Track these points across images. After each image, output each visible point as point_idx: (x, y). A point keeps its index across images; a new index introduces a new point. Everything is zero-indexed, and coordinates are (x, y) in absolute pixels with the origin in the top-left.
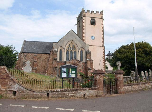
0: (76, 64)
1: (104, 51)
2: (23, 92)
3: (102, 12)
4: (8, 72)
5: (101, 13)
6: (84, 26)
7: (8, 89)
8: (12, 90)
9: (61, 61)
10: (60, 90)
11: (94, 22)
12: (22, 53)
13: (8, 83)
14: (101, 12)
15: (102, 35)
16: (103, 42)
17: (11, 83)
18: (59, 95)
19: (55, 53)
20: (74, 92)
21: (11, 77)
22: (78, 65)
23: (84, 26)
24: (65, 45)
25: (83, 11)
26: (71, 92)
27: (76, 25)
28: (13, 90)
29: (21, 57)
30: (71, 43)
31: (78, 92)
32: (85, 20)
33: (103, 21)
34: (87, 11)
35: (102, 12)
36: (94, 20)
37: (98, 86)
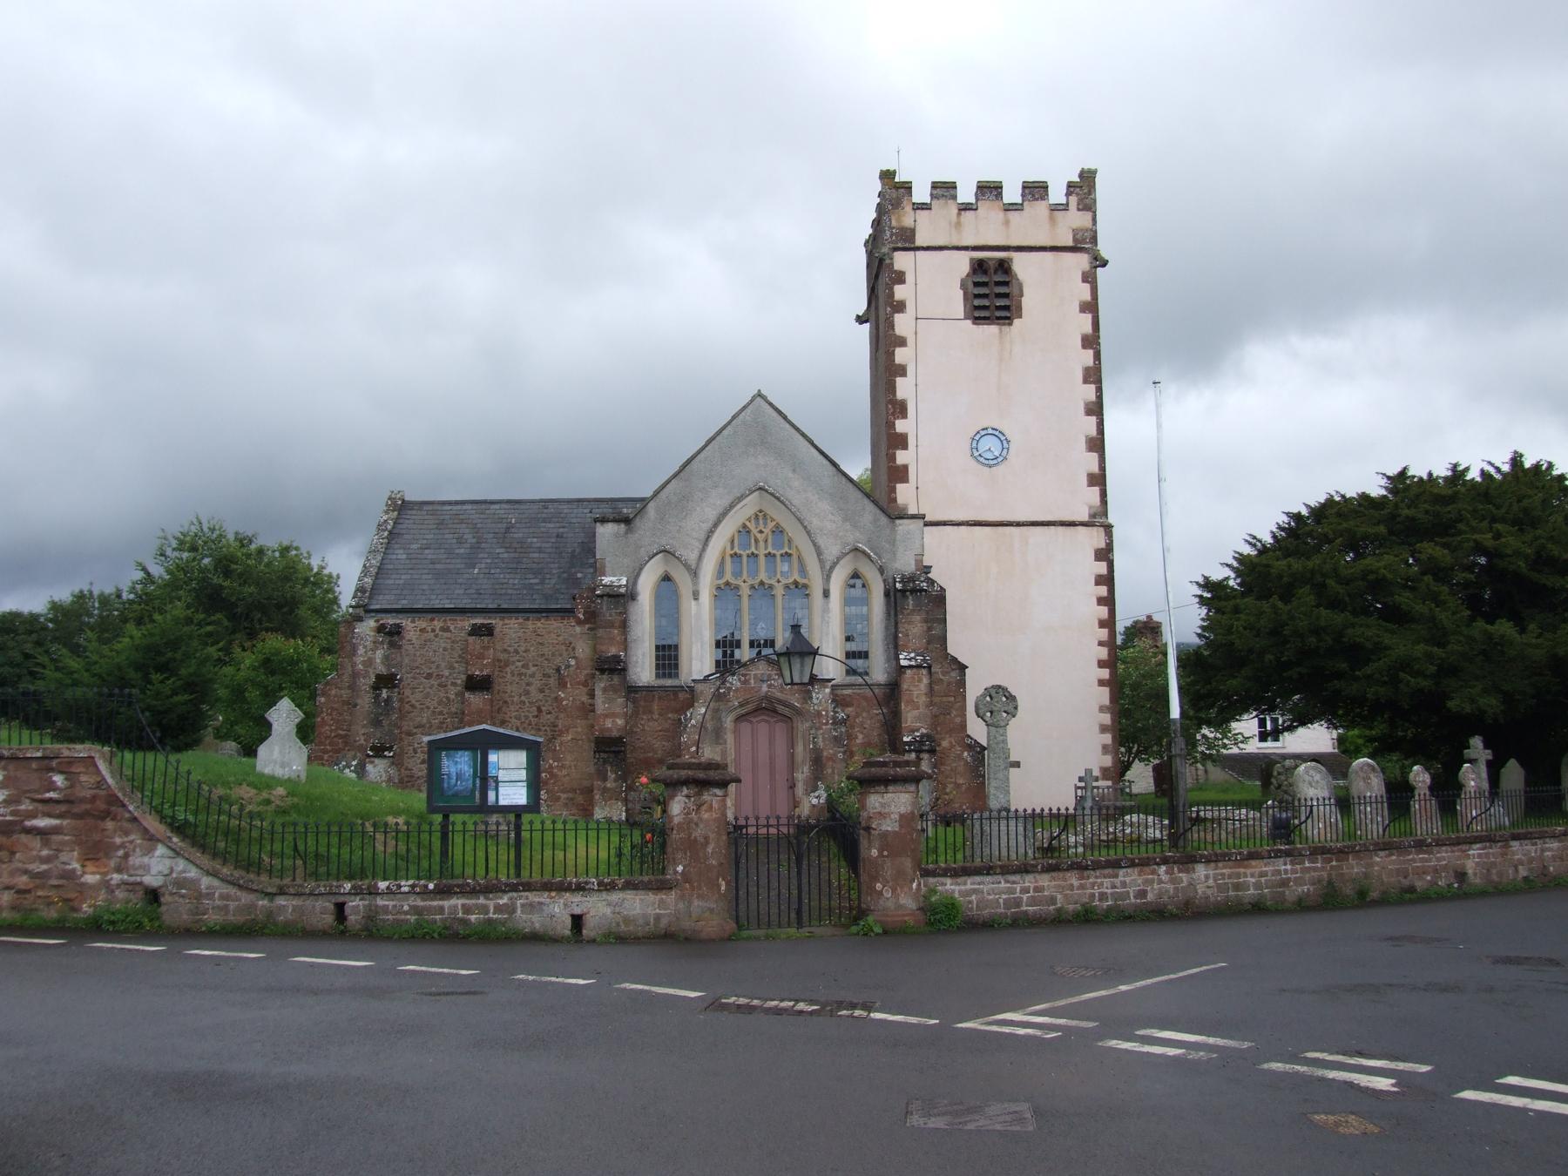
0: (780, 702)
1: (1102, 568)
2: (200, 893)
3: (1084, 187)
4: (110, 780)
5: (1073, 200)
6: (902, 342)
7: (116, 877)
8: (138, 879)
9: (669, 682)
10: (413, 886)
11: (999, 296)
12: (368, 611)
13: (118, 840)
14: (1070, 185)
15: (1089, 412)
16: (1098, 479)
17: (131, 842)
18: (406, 913)
19: (607, 612)
20: (504, 900)
21: (131, 808)
22: (799, 712)
23: (902, 342)
24: (703, 536)
25: (894, 190)
26: (482, 901)
27: (860, 320)
28: (140, 883)
29: (361, 651)
30: (761, 515)
31: (531, 905)
32: (909, 278)
33: (1089, 278)
34: (935, 186)
35: (1084, 187)
36: (1004, 267)
37: (680, 868)
